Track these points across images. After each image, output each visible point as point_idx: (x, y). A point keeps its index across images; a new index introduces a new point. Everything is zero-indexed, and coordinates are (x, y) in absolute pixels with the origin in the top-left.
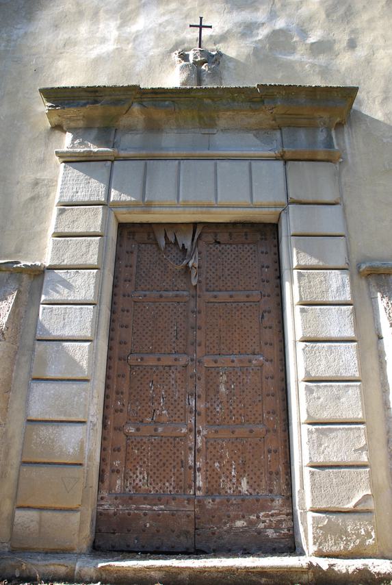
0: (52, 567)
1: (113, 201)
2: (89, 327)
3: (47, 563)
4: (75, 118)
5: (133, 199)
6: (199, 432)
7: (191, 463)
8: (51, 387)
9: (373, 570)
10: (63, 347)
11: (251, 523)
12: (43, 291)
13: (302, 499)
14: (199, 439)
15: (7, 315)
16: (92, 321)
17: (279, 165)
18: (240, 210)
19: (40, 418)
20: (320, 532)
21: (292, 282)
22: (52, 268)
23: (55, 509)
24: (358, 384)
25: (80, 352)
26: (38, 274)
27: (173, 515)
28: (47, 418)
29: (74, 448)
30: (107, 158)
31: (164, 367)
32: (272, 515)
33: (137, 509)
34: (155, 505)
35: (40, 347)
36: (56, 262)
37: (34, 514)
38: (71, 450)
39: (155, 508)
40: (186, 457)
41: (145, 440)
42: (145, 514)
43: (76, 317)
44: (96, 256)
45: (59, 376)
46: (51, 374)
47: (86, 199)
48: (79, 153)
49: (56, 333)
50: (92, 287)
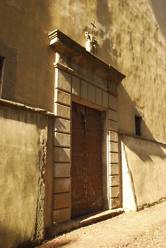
0: (69, 227)
1: (73, 93)
2: (70, 143)
3: (67, 226)
4: (62, 48)
5: (77, 94)
6: (86, 178)
7: (84, 187)
8: (61, 165)
9: (117, 211)
10: (63, 150)
11: (96, 203)
12: (55, 126)
13: (109, 195)
14: (86, 180)
15: (47, 135)
16: (70, 141)
17: (107, 94)
18: (98, 107)
19: (58, 177)
20: (112, 203)
21: (108, 135)
22: (58, 117)
23: (63, 208)
24: (118, 165)
25: (68, 151)
26: (53, 118)
27: (82, 204)
28: (60, 176)
29: (68, 187)
30: (70, 73)
31: (78, 156)
32: (99, 200)
33: (74, 204)
34: (78, 202)
35: (56, 149)
36: (59, 115)
37: (59, 211)
38: (67, 187)
39: (78, 202)
40: (83, 186)
41: (74, 181)
42: (76, 205)
43: (66, 139)
44: (70, 115)
45: (62, 161)
46: (61, 160)
47: (66, 89)
48: (65, 67)
49: (61, 144)
50: (70, 127)
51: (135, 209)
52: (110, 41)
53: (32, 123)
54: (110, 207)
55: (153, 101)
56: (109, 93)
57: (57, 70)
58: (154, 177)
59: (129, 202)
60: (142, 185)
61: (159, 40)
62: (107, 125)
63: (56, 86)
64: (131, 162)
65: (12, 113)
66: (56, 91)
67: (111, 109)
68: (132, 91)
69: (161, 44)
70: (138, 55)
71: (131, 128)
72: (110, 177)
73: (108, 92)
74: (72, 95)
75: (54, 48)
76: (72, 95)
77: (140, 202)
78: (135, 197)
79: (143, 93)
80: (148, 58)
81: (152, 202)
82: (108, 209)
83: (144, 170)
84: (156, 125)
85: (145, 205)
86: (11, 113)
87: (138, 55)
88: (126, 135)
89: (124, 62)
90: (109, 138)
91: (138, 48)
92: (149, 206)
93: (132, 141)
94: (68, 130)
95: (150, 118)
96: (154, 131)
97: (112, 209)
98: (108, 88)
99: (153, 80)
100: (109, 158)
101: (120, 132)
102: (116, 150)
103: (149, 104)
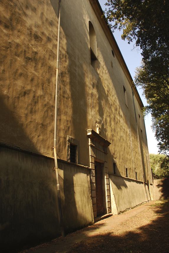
18: (146, 164)
51: (117, 213)
52: (68, 58)
53: (86, 174)
54: (108, 213)
55: (120, 153)
56: (105, 153)
57: (90, 147)
58: (123, 197)
59: (114, 210)
60: (119, 201)
61: (121, 114)
62: (105, 170)
63: (90, 155)
64: (114, 189)
65: (75, 170)
66: (90, 157)
67: (106, 162)
68: (111, 150)
69: (121, 117)
70: (113, 128)
71: (112, 171)
72: (107, 197)
73: (104, 153)
74: (95, 158)
75: (89, 136)
76: (95, 158)
77: (119, 211)
78: (117, 207)
79: (116, 149)
80: (117, 128)
81: (123, 210)
82: (107, 213)
83: (118, 193)
84: (121, 167)
85: (121, 212)
86: (74, 170)
87: (113, 128)
88: (111, 174)
89: (108, 134)
90: (105, 177)
91: (113, 123)
92: (122, 212)
93: (113, 177)
94: (94, 175)
95: (119, 163)
96: (121, 170)
97: (108, 213)
98: (104, 151)
99: (119, 140)
100: (106, 188)
101: (109, 173)
102: (108, 183)
103: (118, 155)
